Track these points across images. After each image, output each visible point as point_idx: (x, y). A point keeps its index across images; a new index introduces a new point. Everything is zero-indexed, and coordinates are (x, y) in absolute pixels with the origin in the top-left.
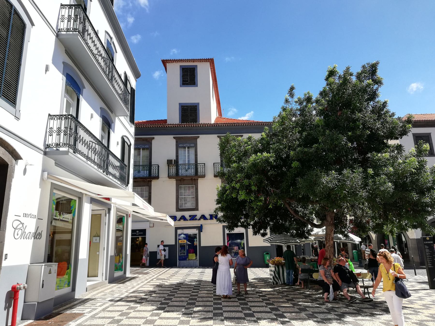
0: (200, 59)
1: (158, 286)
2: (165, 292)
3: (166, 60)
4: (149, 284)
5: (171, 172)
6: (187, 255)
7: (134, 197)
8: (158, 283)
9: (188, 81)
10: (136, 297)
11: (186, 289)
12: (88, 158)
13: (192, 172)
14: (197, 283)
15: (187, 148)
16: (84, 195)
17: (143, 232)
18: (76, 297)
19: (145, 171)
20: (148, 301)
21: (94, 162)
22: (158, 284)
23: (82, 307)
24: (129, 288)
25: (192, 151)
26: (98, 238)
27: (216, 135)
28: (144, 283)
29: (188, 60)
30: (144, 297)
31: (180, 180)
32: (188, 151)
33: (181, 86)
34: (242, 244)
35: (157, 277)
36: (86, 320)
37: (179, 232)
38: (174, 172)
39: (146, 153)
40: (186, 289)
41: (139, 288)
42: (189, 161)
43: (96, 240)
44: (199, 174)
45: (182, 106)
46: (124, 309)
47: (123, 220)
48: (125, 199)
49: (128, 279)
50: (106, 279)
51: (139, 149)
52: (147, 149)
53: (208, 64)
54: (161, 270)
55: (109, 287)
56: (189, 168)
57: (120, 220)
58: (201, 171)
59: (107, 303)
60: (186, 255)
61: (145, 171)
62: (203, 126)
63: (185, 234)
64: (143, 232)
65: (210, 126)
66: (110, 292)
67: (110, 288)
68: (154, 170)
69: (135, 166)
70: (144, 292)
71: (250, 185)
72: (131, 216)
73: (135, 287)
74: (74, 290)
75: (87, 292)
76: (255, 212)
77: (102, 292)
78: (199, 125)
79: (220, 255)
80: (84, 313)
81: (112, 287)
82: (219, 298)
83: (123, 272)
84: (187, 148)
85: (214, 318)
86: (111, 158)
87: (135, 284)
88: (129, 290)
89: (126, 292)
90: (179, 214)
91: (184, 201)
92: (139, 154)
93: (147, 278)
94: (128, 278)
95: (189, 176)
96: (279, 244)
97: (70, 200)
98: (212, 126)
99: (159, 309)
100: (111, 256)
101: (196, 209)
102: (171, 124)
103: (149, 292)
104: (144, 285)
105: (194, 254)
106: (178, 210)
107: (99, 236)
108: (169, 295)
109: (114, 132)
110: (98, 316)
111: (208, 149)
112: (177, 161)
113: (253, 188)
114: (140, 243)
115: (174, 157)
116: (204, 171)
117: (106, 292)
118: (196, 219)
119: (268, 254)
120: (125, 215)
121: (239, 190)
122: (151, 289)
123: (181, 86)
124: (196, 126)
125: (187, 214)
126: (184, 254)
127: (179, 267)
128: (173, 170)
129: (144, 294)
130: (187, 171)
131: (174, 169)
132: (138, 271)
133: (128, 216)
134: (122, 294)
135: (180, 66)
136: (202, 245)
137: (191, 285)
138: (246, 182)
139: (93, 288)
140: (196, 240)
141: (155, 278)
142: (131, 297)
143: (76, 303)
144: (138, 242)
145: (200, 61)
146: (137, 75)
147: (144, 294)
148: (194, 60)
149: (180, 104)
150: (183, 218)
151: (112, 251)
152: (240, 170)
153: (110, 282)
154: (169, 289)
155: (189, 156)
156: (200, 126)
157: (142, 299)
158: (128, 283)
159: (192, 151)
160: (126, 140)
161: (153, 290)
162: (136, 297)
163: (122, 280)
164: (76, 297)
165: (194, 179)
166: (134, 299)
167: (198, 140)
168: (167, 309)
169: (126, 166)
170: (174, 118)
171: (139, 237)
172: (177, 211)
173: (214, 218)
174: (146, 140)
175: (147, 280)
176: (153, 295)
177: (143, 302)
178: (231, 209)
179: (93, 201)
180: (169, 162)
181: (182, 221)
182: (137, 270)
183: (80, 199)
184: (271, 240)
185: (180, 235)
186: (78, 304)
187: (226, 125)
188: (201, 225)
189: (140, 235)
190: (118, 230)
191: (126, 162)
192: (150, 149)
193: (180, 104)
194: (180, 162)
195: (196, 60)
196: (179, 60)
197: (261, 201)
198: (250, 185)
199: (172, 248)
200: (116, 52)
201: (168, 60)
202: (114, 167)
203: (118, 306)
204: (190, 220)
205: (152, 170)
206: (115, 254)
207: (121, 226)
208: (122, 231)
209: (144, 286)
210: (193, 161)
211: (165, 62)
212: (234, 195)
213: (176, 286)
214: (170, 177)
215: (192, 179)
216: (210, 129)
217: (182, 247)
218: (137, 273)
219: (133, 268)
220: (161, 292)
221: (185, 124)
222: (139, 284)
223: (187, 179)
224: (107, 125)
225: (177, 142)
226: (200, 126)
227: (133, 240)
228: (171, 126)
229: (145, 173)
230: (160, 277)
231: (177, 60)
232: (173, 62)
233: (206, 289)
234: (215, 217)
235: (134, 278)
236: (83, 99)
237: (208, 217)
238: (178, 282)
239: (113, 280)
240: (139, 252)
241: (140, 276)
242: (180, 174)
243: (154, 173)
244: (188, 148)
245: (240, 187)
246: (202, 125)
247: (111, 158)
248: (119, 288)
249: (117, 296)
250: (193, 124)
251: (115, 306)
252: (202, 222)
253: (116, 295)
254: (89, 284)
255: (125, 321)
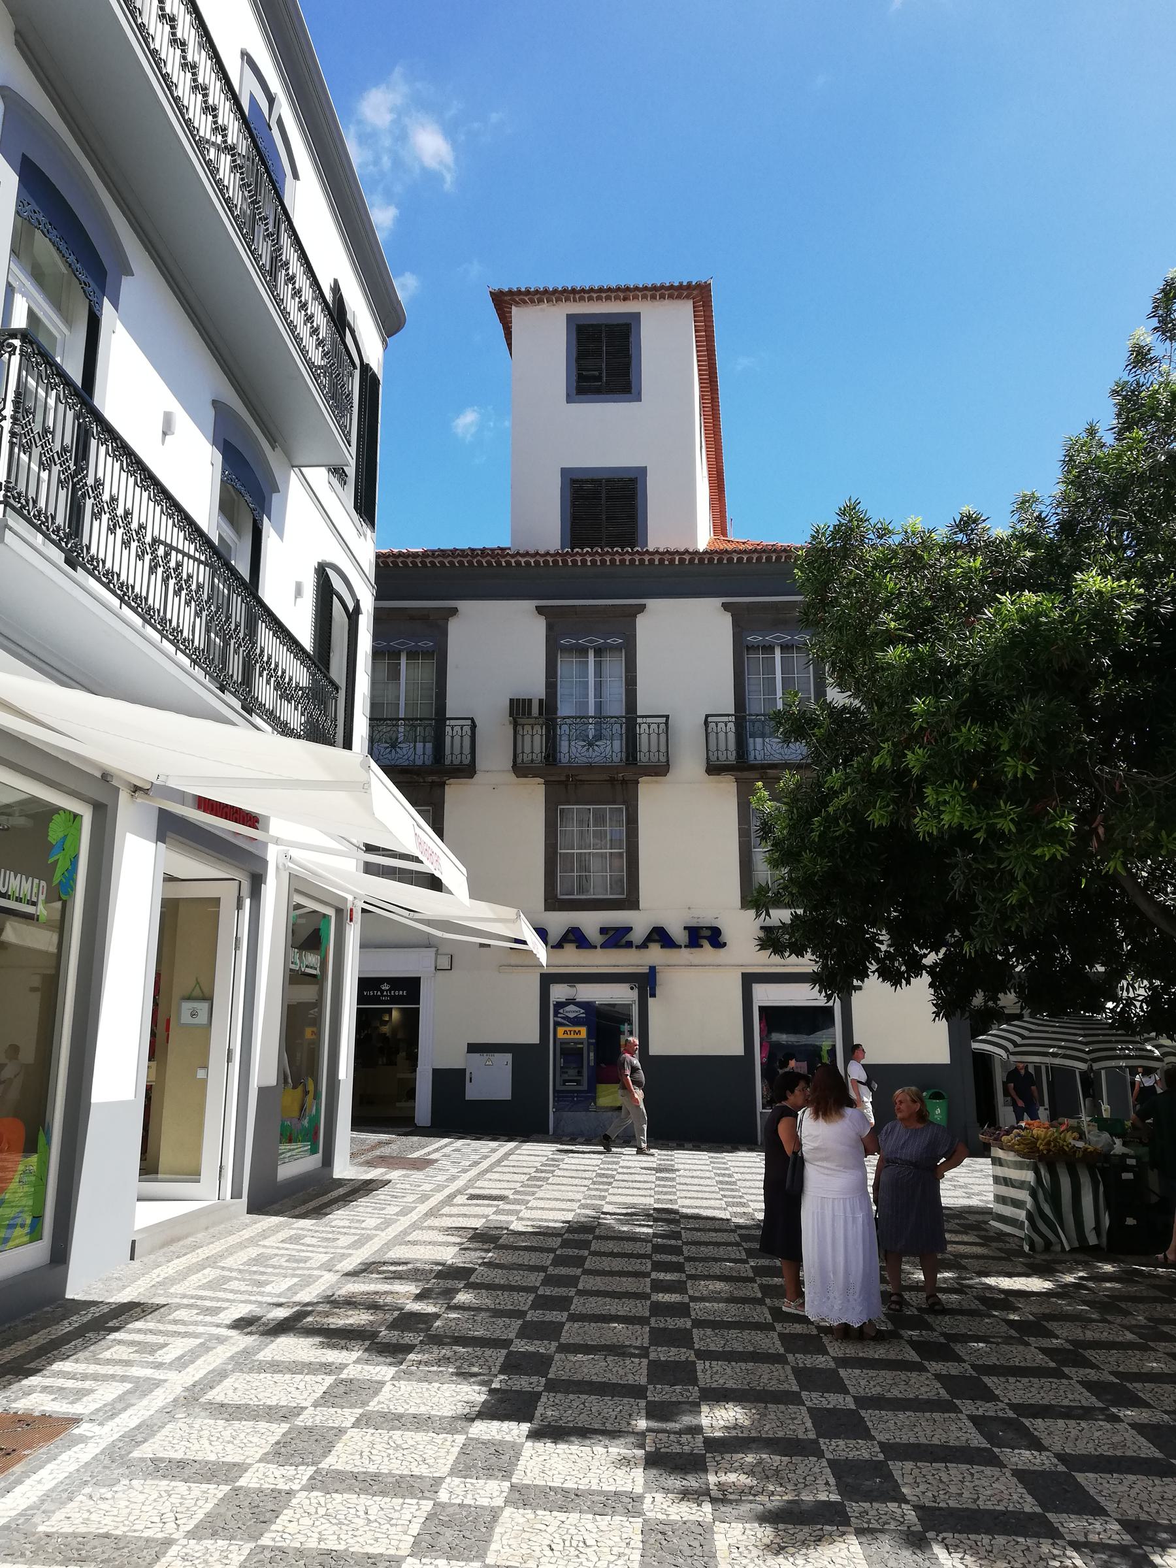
0: (654, 288)
1: (484, 1238)
2: (516, 1278)
3: (510, 292)
4: (436, 1222)
5: (527, 749)
6: (592, 1089)
7: (366, 787)
8: (479, 1217)
9: (599, 378)
10: (373, 1307)
11: (617, 1264)
12: (125, 594)
13: (611, 750)
14: (662, 1228)
15: (591, 654)
16: (124, 796)
17: (409, 988)
18: (74, 1291)
19: (420, 745)
20: (437, 1340)
21: (174, 636)
22: (478, 1223)
23: (81, 1368)
24: (344, 1241)
25: (615, 666)
26: (203, 1007)
27: (717, 602)
28: (414, 1216)
29: (601, 290)
30: (417, 1307)
31: (564, 783)
32: (599, 665)
33: (569, 400)
34: (824, 1054)
35: (471, 1183)
36: (65, 1493)
37: (559, 992)
38: (537, 749)
39: (424, 672)
40: (617, 1264)
41: (389, 1245)
42: (599, 706)
43: (193, 1014)
44: (643, 758)
45: (573, 481)
46: (304, 1391)
47: (324, 941)
48: (329, 816)
49: (341, 1191)
50: (236, 1194)
51: (396, 655)
52: (427, 654)
53: (684, 310)
54: (485, 1151)
55: (247, 1234)
56: (599, 737)
57: (309, 935)
58: (654, 749)
59: (221, 1340)
60: (585, 1087)
61: (420, 745)
62: (661, 561)
63: (580, 1005)
64: (409, 988)
65: (691, 561)
66: (248, 1263)
67: (253, 1241)
68: (457, 739)
69: (375, 721)
70: (415, 1275)
71: (990, 754)
72: (358, 915)
73: (370, 1238)
74: (60, 1254)
75: (136, 1264)
76: (1013, 898)
77: (211, 1262)
78: (647, 558)
79: (806, 1117)
80: (76, 1420)
81: (264, 1235)
82: (814, 1338)
83: (319, 1156)
84: (591, 654)
85: (854, 1508)
86: (266, 638)
87: (371, 1222)
88: (344, 1256)
89: (328, 1267)
90: (560, 921)
91: (580, 869)
92: (394, 675)
93: (427, 1187)
94: (340, 1183)
95: (603, 768)
96: (1057, 1061)
97: (43, 814)
98: (701, 560)
99: (503, 1407)
100: (262, 1091)
101: (631, 902)
102: (527, 554)
103: (440, 1275)
104: (415, 1226)
105: (614, 1088)
106: (553, 902)
107: (208, 998)
108: (542, 1303)
109: (280, 533)
110: (146, 1451)
111: (685, 657)
112: (549, 705)
113: (1014, 768)
114: (394, 1031)
115: (536, 689)
116: (663, 749)
117: (229, 1262)
118: (629, 945)
119: (937, 1096)
120: (331, 912)
121: (921, 781)
122: (449, 1255)
123: (569, 400)
124: (632, 561)
125: (591, 922)
126: (578, 1082)
127: (556, 1138)
128: (534, 742)
129: (413, 1289)
130: (591, 744)
131: (537, 738)
132: (385, 1151)
133: (343, 914)
134: (307, 1281)
135: (570, 318)
136: (655, 1049)
137: (633, 1238)
138: (971, 735)
139: (170, 1237)
140: (626, 1027)
141: (459, 1192)
142: (350, 1303)
143: (65, 1327)
144: (385, 1029)
145: (653, 297)
146: (390, 319)
147: (413, 1289)
148: (627, 289)
149: (564, 471)
150: (575, 938)
151: (265, 1066)
152: (933, 678)
153: (257, 1207)
154: (533, 1259)
155: (599, 686)
156: (651, 561)
157: (406, 1321)
158: (339, 1217)
159: (615, 666)
160: (337, 584)
161: (459, 1262)
162: (373, 1307)
163: (315, 1196)
164: (74, 1291)
165: (624, 782)
166: (359, 1318)
167: (641, 621)
168: (546, 1410)
169: (337, 688)
170: (545, 529)
171: (391, 1010)
172: (548, 908)
173: (706, 943)
174: (423, 617)
175: (424, 1198)
176: (463, 1297)
177: (409, 1349)
178: (845, 885)
179: (169, 828)
180: (519, 709)
181: (570, 948)
182: (381, 1144)
183: (104, 814)
184: (1015, 1044)
185: (559, 1005)
186: (67, 1339)
187: (759, 559)
188: (653, 969)
189: (395, 1000)
190: (294, 978)
191: (337, 671)
192: (438, 656)
193: (564, 471)
194: (565, 709)
195: (636, 288)
196: (565, 291)
197: (1058, 835)
198: (990, 754)
199: (525, 1058)
200: (296, 176)
201: (519, 292)
202: (285, 690)
203: (275, 1367)
204: (602, 946)
205: (448, 739)
206: (283, 1077)
207: (312, 959)
208: (316, 980)
209: (413, 1236)
210: (616, 708)
211: (504, 302)
212: (877, 817)
213: (565, 1244)
214: (521, 769)
215: (612, 781)
216: (690, 575)
217: (570, 1053)
218: (383, 1161)
219: (363, 1136)
220: (498, 1277)
221: (587, 555)
222: (387, 1223)
223: (590, 777)
224: (249, 492)
225: (550, 628)
226: (651, 561)
227: (364, 1020)
228: (528, 563)
229: (419, 751)
230: (487, 1186)
231: (555, 291)
232: (540, 301)
233: (716, 1269)
234: (708, 938)
235: (366, 1188)
236: (119, 327)
237: (677, 932)
238: (569, 1217)
239: (269, 1197)
240: (391, 1066)
241: (395, 1175)
242: (564, 759)
243: (457, 750)
244: (599, 652)
245: (926, 767)
246: (657, 558)
247: (266, 638)
248: (295, 1239)
249: (280, 1292)
250: (618, 555)
251: (262, 1368)
252: (655, 955)
253: (278, 1287)
254: (148, 1215)
255: (304, 1525)
